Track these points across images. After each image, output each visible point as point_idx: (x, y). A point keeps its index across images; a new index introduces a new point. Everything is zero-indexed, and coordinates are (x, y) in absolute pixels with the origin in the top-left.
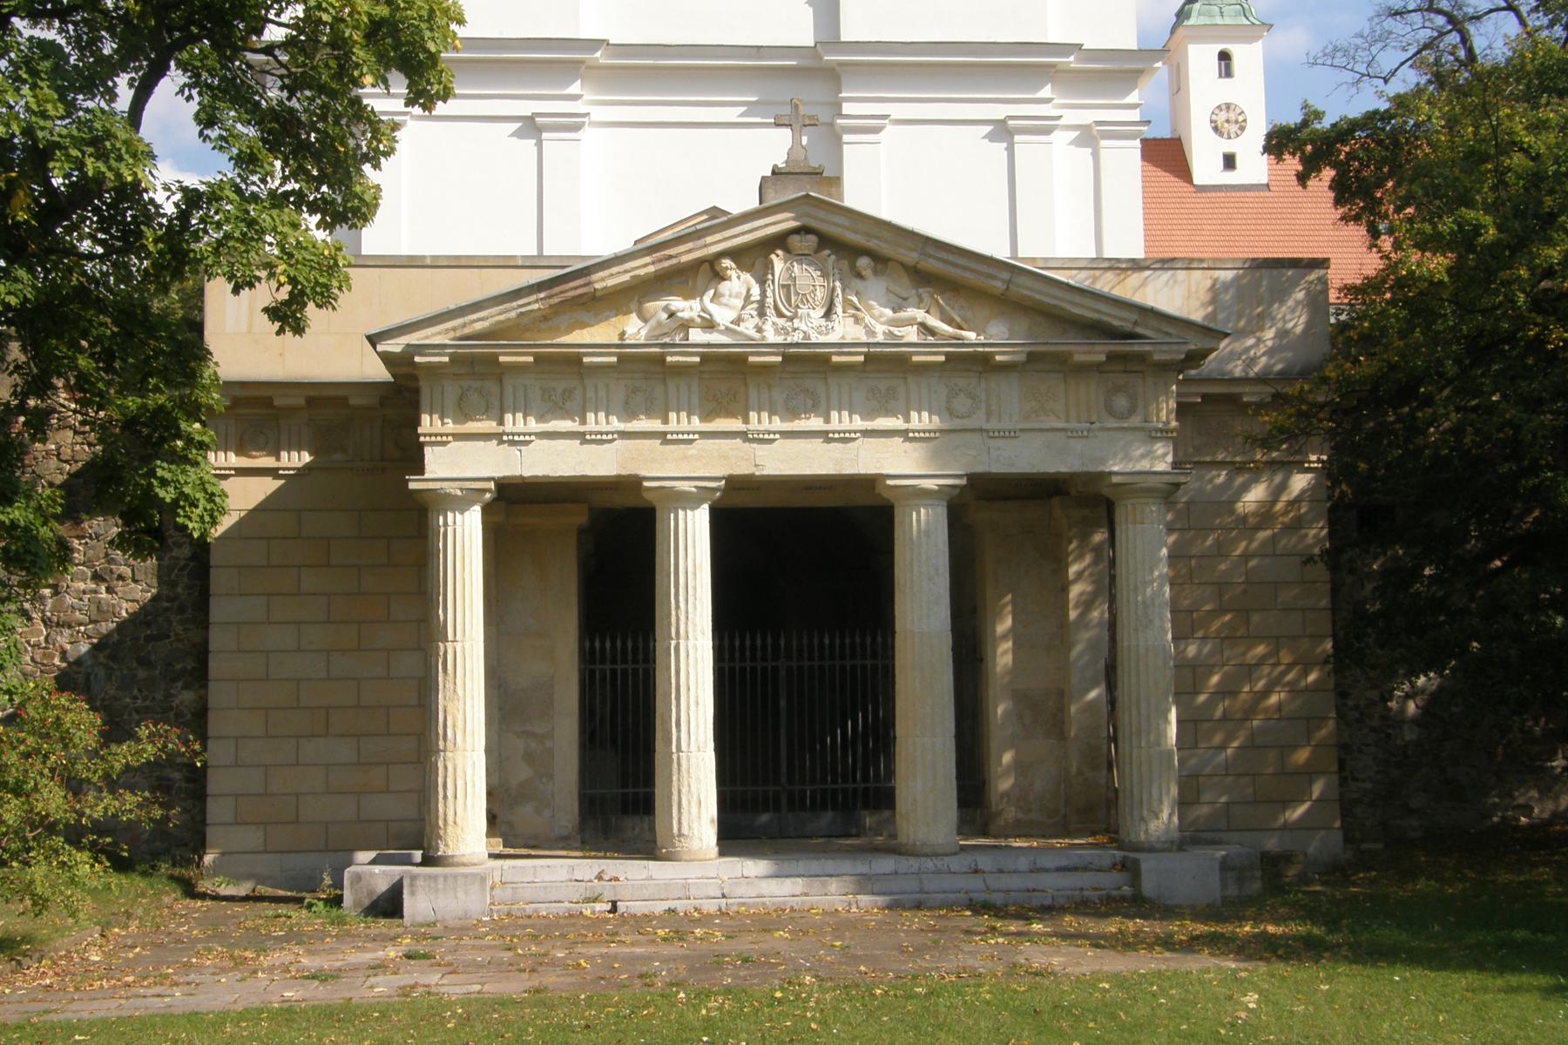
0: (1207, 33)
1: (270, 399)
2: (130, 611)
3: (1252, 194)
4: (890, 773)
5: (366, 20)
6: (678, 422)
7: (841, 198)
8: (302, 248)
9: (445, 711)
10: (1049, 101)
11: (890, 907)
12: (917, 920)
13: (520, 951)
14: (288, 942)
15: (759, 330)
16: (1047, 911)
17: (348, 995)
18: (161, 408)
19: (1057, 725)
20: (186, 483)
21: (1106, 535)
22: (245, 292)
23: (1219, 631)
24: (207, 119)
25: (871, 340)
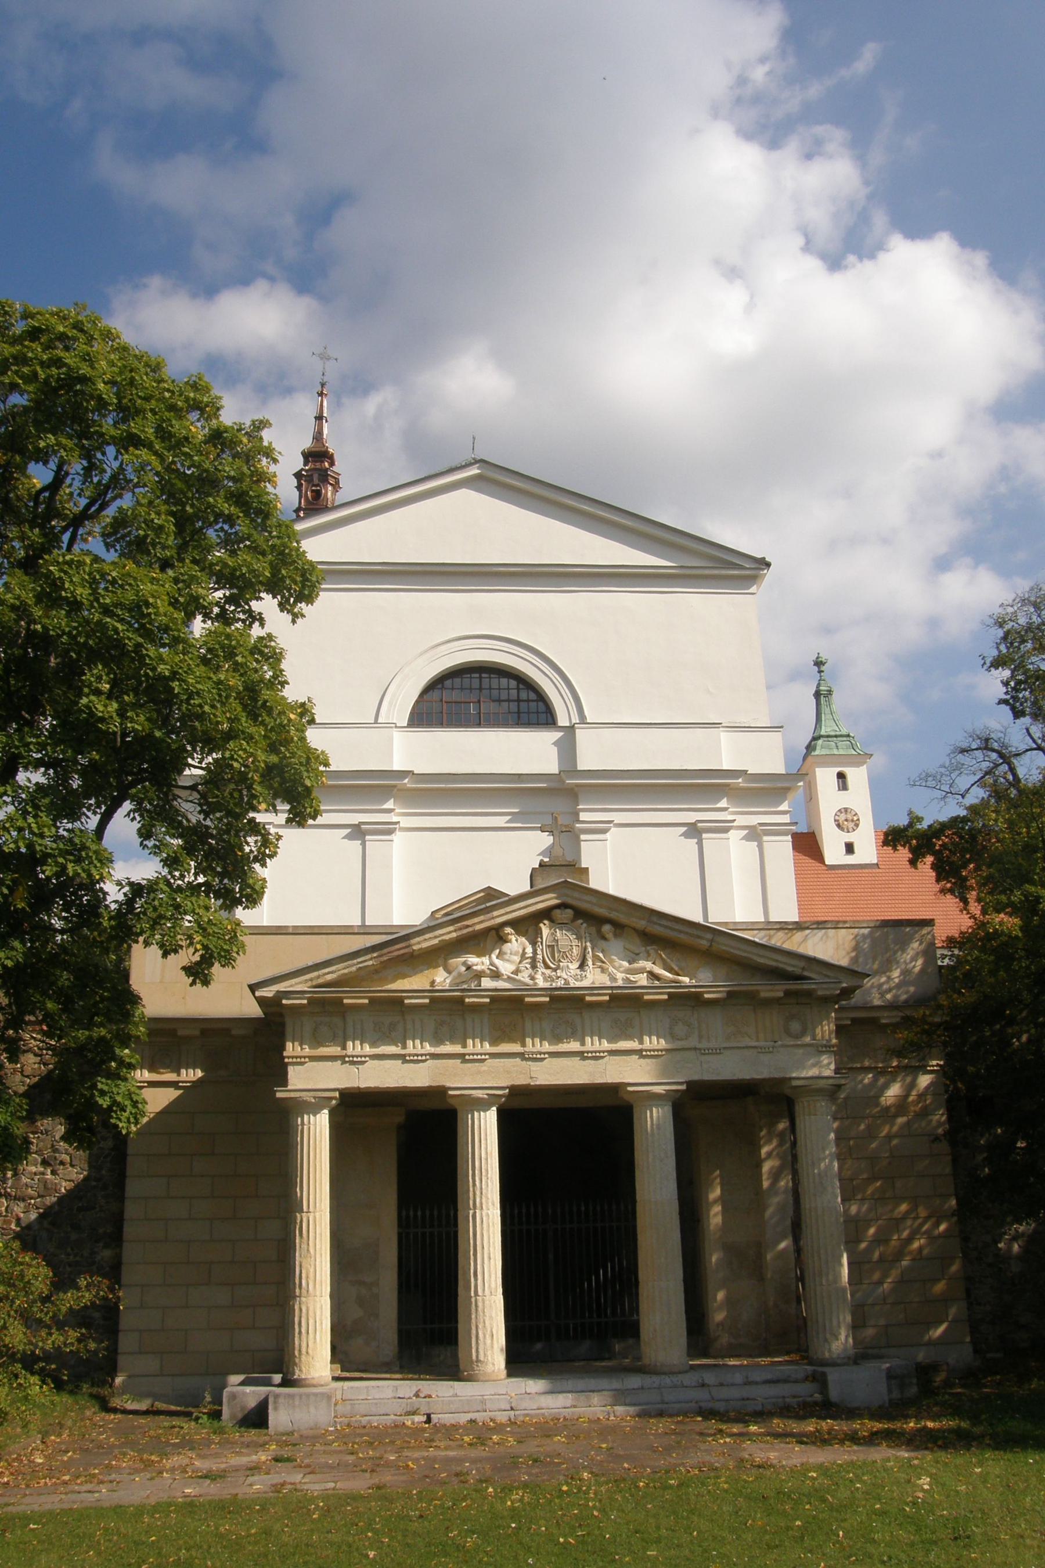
0: (828, 761)
1: (175, 1030)
2: (68, 1188)
3: (867, 871)
4: (635, 1309)
5: (263, 765)
6: (474, 1046)
7: (588, 882)
8: (213, 924)
9: (301, 1266)
10: (725, 810)
11: (639, 1415)
12: (661, 1425)
13: (361, 1455)
14: (183, 1448)
15: (532, 978)
16: (761, 1415)
17: (234, 1492)
18: (102, 1039)
19: (757, 1269)
20: (118, 1094)
21: (788, 1124)
22: (172, 957)
23: (873, 1194)
24: (145, 834)
25: (614, 985)
